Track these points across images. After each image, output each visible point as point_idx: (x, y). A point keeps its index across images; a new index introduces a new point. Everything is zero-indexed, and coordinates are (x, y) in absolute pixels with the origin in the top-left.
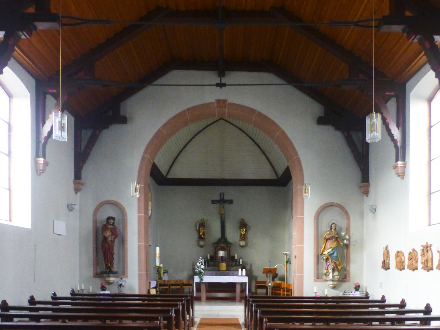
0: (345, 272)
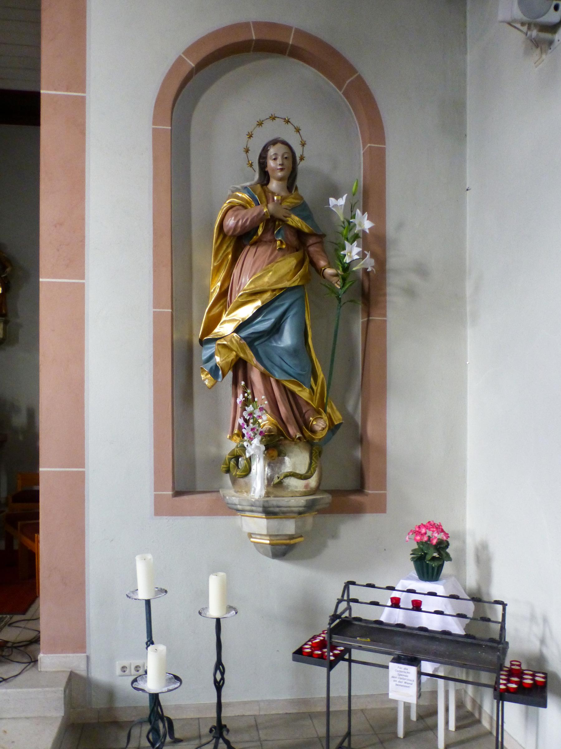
0: (358, 453)
